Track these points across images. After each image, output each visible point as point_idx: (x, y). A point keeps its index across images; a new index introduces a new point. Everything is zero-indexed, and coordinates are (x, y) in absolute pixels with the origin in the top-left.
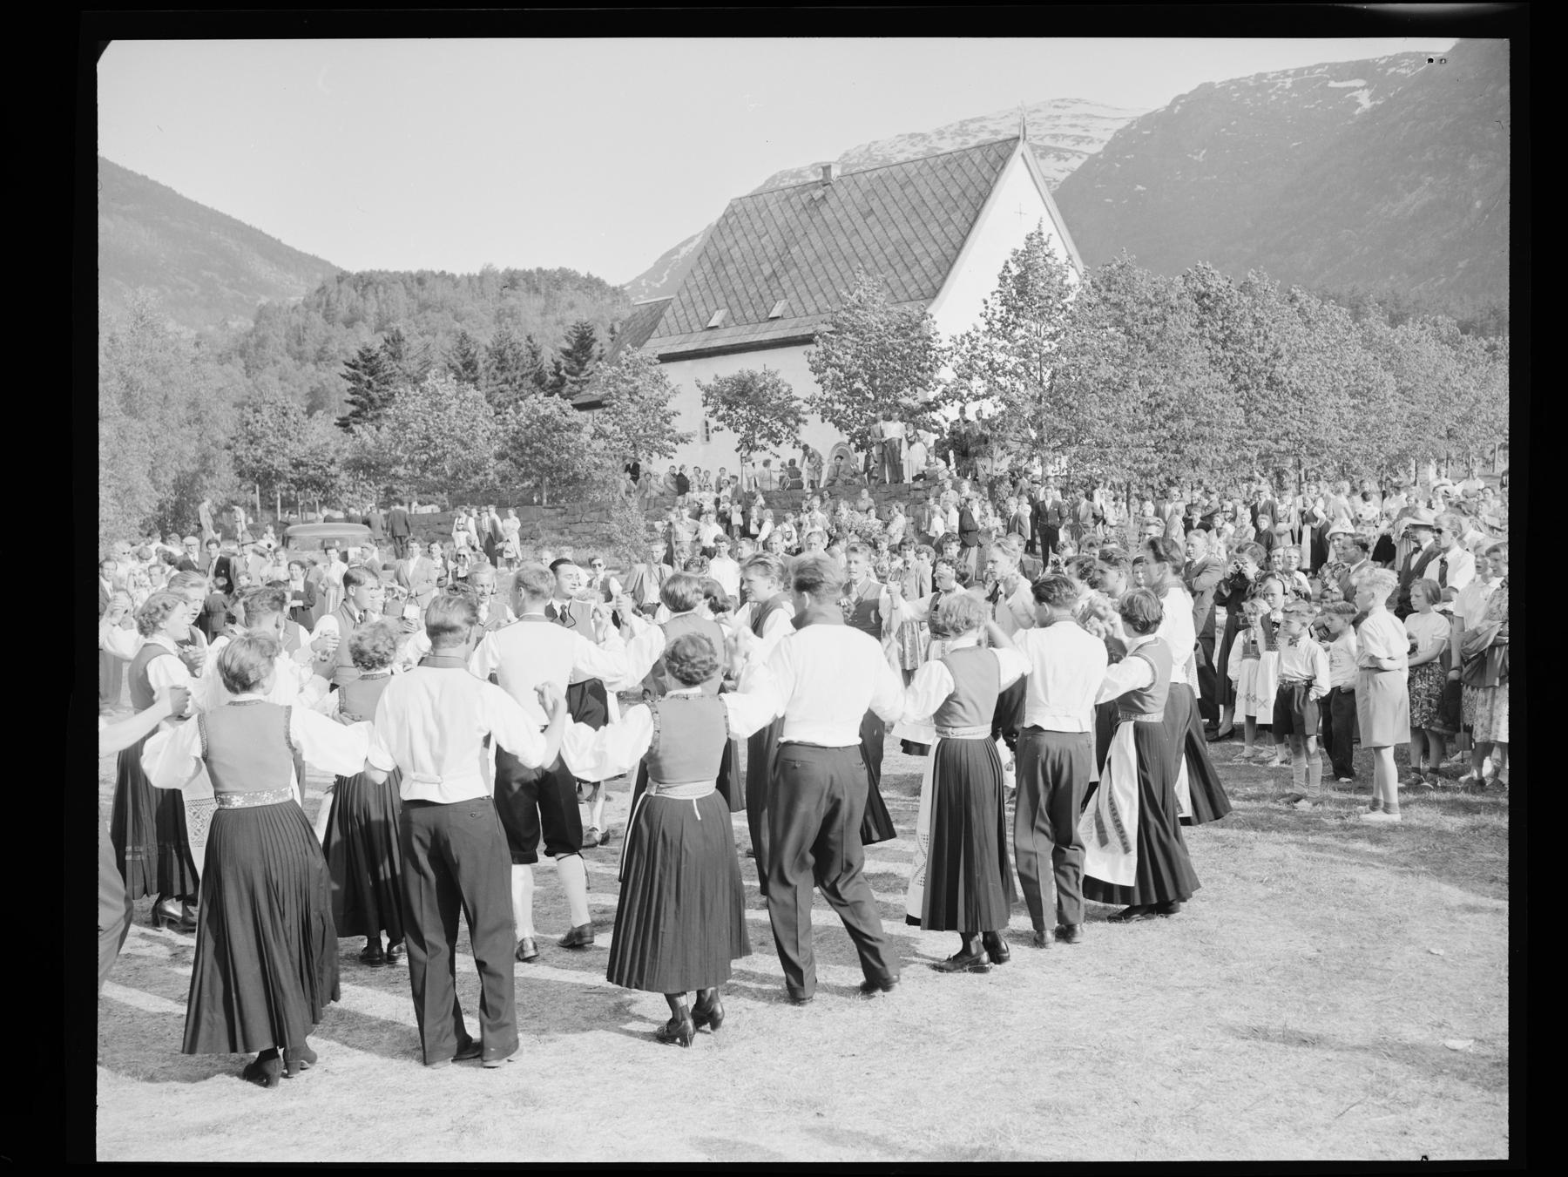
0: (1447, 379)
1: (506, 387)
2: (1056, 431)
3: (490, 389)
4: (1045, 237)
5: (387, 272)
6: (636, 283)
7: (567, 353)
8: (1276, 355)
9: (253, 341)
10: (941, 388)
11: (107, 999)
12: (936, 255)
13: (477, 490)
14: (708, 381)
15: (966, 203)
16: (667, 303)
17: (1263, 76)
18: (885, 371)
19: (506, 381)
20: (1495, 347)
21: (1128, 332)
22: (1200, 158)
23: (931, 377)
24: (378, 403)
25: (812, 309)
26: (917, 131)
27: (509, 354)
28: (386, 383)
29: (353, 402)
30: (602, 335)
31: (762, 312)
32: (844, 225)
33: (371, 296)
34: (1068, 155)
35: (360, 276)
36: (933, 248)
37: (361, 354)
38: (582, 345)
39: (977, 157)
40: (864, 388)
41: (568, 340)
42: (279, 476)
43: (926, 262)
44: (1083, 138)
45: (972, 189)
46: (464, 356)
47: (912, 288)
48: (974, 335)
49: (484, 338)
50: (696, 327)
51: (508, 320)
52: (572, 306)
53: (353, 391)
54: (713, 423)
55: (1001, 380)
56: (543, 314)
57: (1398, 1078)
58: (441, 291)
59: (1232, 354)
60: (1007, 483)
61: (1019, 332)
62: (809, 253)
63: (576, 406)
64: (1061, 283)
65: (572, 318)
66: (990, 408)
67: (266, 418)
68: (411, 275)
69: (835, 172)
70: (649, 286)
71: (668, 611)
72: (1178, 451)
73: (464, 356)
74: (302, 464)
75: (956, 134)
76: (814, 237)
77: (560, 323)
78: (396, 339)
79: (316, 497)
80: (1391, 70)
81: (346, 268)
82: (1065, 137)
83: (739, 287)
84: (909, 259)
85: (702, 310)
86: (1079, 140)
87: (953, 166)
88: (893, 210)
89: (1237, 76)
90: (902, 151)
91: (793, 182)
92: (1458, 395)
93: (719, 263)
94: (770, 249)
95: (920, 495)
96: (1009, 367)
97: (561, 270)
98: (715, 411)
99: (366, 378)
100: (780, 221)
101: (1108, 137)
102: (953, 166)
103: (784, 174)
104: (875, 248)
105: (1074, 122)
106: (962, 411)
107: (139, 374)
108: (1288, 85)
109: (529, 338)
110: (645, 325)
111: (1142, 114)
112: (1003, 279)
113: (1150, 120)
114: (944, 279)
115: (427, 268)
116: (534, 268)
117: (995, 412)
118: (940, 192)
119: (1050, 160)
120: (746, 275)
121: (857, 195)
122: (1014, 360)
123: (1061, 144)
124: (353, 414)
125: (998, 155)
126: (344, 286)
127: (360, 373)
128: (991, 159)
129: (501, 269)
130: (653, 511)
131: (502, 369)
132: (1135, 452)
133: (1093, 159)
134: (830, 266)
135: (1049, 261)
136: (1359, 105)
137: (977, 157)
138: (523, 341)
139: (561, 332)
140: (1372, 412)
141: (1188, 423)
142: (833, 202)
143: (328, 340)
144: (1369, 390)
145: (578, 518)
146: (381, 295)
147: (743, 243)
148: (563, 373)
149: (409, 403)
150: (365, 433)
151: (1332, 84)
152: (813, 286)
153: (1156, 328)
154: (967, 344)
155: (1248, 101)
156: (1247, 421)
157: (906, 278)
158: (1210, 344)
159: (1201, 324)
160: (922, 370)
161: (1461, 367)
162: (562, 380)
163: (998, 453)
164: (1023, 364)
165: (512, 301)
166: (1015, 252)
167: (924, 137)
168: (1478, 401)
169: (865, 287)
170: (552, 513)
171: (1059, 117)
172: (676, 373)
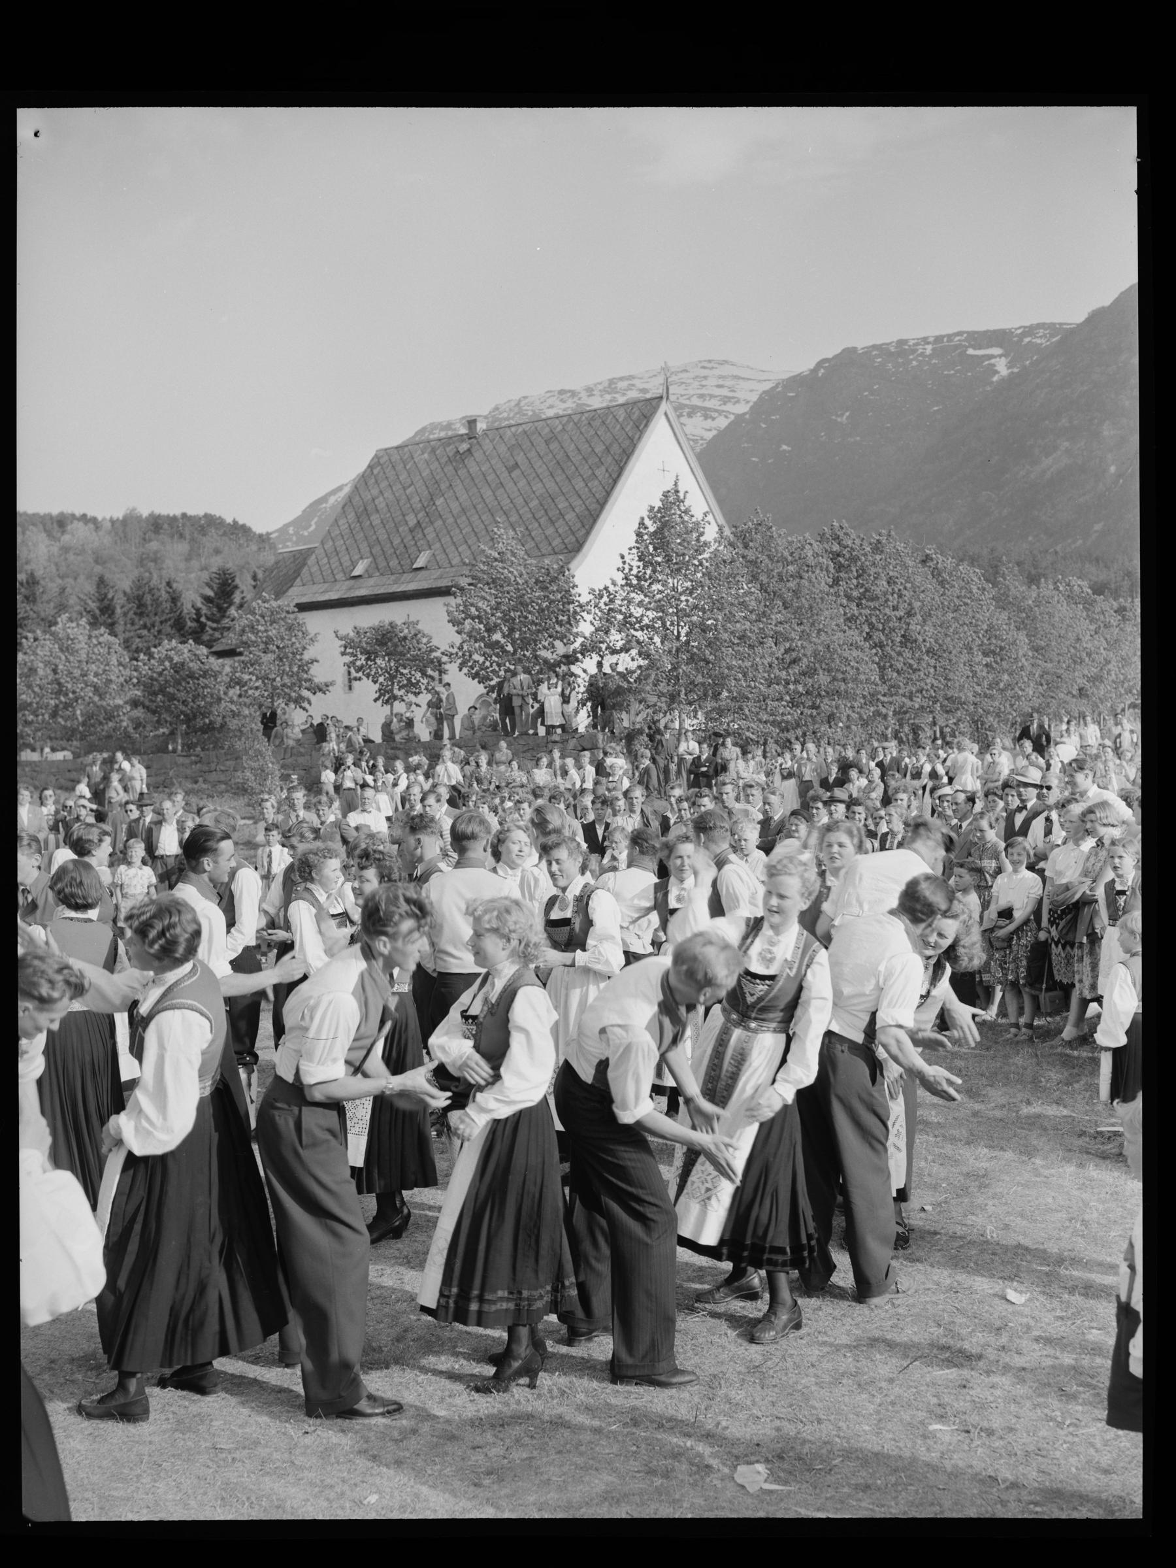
0: (1078, 640)
1: (145, 632)
2: (692, 686)
3: (128, 635)
4: (681, 495)
6: (283, 530)
7: (208, 600)
8: (910, 614)
10: (580, 640)
13: (109, 737)
14: (347, 630)
15: (610, 459)
16: (310, 551)
18: (524, 624)
20: (1125, 609)
21: (763, 588)
23: (569, 630)
26: (567, 388)
27: (148, 599)
30: (244, 584)
32: (489, 478)
34: (715, 415)
36: (577, 503)
38: (224, 590)
40: (503, 641)
43: (570, 516)
45: (616, 446)
48: (612, 589)
49: (123, 583)
50: (340, 576)
51: (152, 564)
52: (217, 552)
55: (639, 634)
56: (188, 559)
57: (964, 1332)
58: (79, 534)
61: (656, 587)
62: (454, 506)
64: (698, 540)
65: (216, 563)
66: (627, 662)
68: (50, 516)
69: (481, 426)
70: (296, 533)
72: (814, 707)
75: (605, 391)
76: (459, 488)
80: (1027, 340)
82: (712, 396)
83: (383, 536)
84: (553, 513)
85: (346, 560)
86: (726, 400)
87: (597, 423)
88: (538, 464)
89: (879, 342)
91: (443, 434)
92: (1089, 655)
93: (363, 513)
96: (646, 621)
97: (206, 515)
101: (754, 398)
102: (597, 423)
103: (433, 427)
104: (519, 501)
105: (721, 382)
106: (600, 665)
108: (928, 352)
109: (169, 584)
110: (291, 569)
111: (786, 376)
112: (639, 534)
114: (588, 533)
117: (633, 665)
118: (585, 447)
119: (698, 419)
121: (502, 449)
123: (708, 404)
125: (642, 414)
128: (635, 417)
130: (289, 761)
133: (739, 418)
134: (475, 518)
135: (686, 518)
136: (997, 372)
137: (621, 415)
139: (205, 576)
140: (1004, 671)
142: (478, 455)
144: (1002, 649)
145: (213, 766)
148: (203, 619)
151: (971, 352)
152: (458, 538)
153: (792, 584)
154: (605, 599)
156: (882, 677)
157: (550, 531)
158: (845, 602)
159: (836, 582)
160: (560, 623)
161: (1093, 627)
162: (203, 626)
163: (635, 706)
164: (660, 618)
165: (154, 545)
166: (652, 509)
167: (573, 394)
168: (1108, 662)
169: (507, 538)
170: (187, 761)
171: (705, 378)
172: (314, 622)
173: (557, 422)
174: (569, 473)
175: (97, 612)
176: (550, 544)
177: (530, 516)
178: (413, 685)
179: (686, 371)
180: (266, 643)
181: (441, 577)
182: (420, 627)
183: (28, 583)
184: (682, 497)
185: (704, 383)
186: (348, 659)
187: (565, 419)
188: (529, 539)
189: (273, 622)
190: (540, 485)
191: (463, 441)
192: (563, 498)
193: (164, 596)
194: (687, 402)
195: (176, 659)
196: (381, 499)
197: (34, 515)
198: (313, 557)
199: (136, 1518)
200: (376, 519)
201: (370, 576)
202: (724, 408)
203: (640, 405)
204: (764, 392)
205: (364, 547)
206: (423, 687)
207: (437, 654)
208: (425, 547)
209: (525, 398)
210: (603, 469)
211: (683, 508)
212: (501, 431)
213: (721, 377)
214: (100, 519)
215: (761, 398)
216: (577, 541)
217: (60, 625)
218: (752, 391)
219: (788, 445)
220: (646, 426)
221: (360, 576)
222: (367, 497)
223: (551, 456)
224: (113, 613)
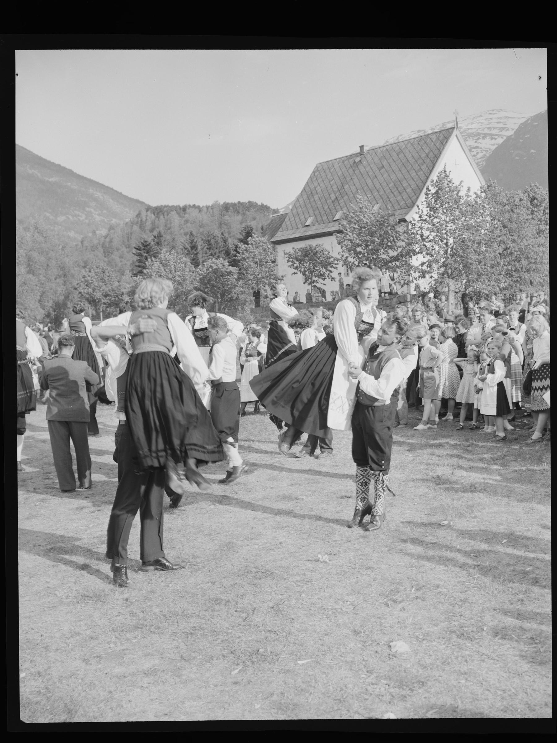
4: (447, 173)
9: (108, 240)
11: (549, 589)
12: (413, 186)
15: (428, 160)
27: (213, 241)
29: (139, 266)
32: (370, 174)
33: (162, 217)
34: (496, 137)
35: (156, 208)
36: (412, 183)
39: (434, 137)
41: (241, 234)
43: (409, 190)
47: (402, 203)
50: (300, 226)
52: (254, 219)
58: (194, 213)
62: (353, 188)
64: (457, 195)
69: (366, 149)
73: (191, 243)
76: (356, 180)
82: (494, 128)
84: (401, 189)
85: (302, 218)
86: (502, 129)
88: (393, 165)
95: (388, 302)
96: (431, 238)
97: (249, 202)
98: (293, 265)
99: (145, 254)
101: (516, 127)
104: (384, 184)
105: (499, 120)
107: (35, 255)
116: (236, 202)
118: (416, 156)
119: (488, 140)
121: (376, 159)
122: (434, 234)
125: (444, 136)
126: (149, 213)
127: (142, 252)
128: (441, 139)
129: (222, 203)
133: (509, 138)
135: (450, 185)
137: (434, 137)
141: (524, 262)
142: (364, 163)
146: (166, 217)
147: (322, 185)
171: (491, 119)
173: (403, 143)
174: (408, 169)
175: (190, 249)
176: (399, 204)
178: (321, 274)
179: (481, 116)
180: (253, 258)
182: (323, 246)
183: (158, 236)
184: (448, 174)
185: (490, 122)
186: (290, 263)
187: (407, 142)
188: (389, 203)
189: (257, 247)
190: (394, 176)
191: (357, 156)
192: (405, 181)
193: (220, 240)
194: (482, 132)
195: (215, 267)
196: (319, 187)
197: (172, 206)
198: (287, 217)
199: (269, 719)
202: (501, 133)
203: (443, 132)
204: (521, 124)
205: (311, 211)
206: (326, 276)
207: (332, 260)
208: (340, 209)
209: (401, 135)
210: (425, 166)
211: (449, 180)
212: (376, 150)
213: (499, 118)
214: (201, 206)
215: (520, 127)
216: (412, 202)
217: (162, 255)
218: (515, 124)
219: (534, 150)
220: (446, 142)
221: (309, 225)
222: (312, 187)
224: (197, 249)
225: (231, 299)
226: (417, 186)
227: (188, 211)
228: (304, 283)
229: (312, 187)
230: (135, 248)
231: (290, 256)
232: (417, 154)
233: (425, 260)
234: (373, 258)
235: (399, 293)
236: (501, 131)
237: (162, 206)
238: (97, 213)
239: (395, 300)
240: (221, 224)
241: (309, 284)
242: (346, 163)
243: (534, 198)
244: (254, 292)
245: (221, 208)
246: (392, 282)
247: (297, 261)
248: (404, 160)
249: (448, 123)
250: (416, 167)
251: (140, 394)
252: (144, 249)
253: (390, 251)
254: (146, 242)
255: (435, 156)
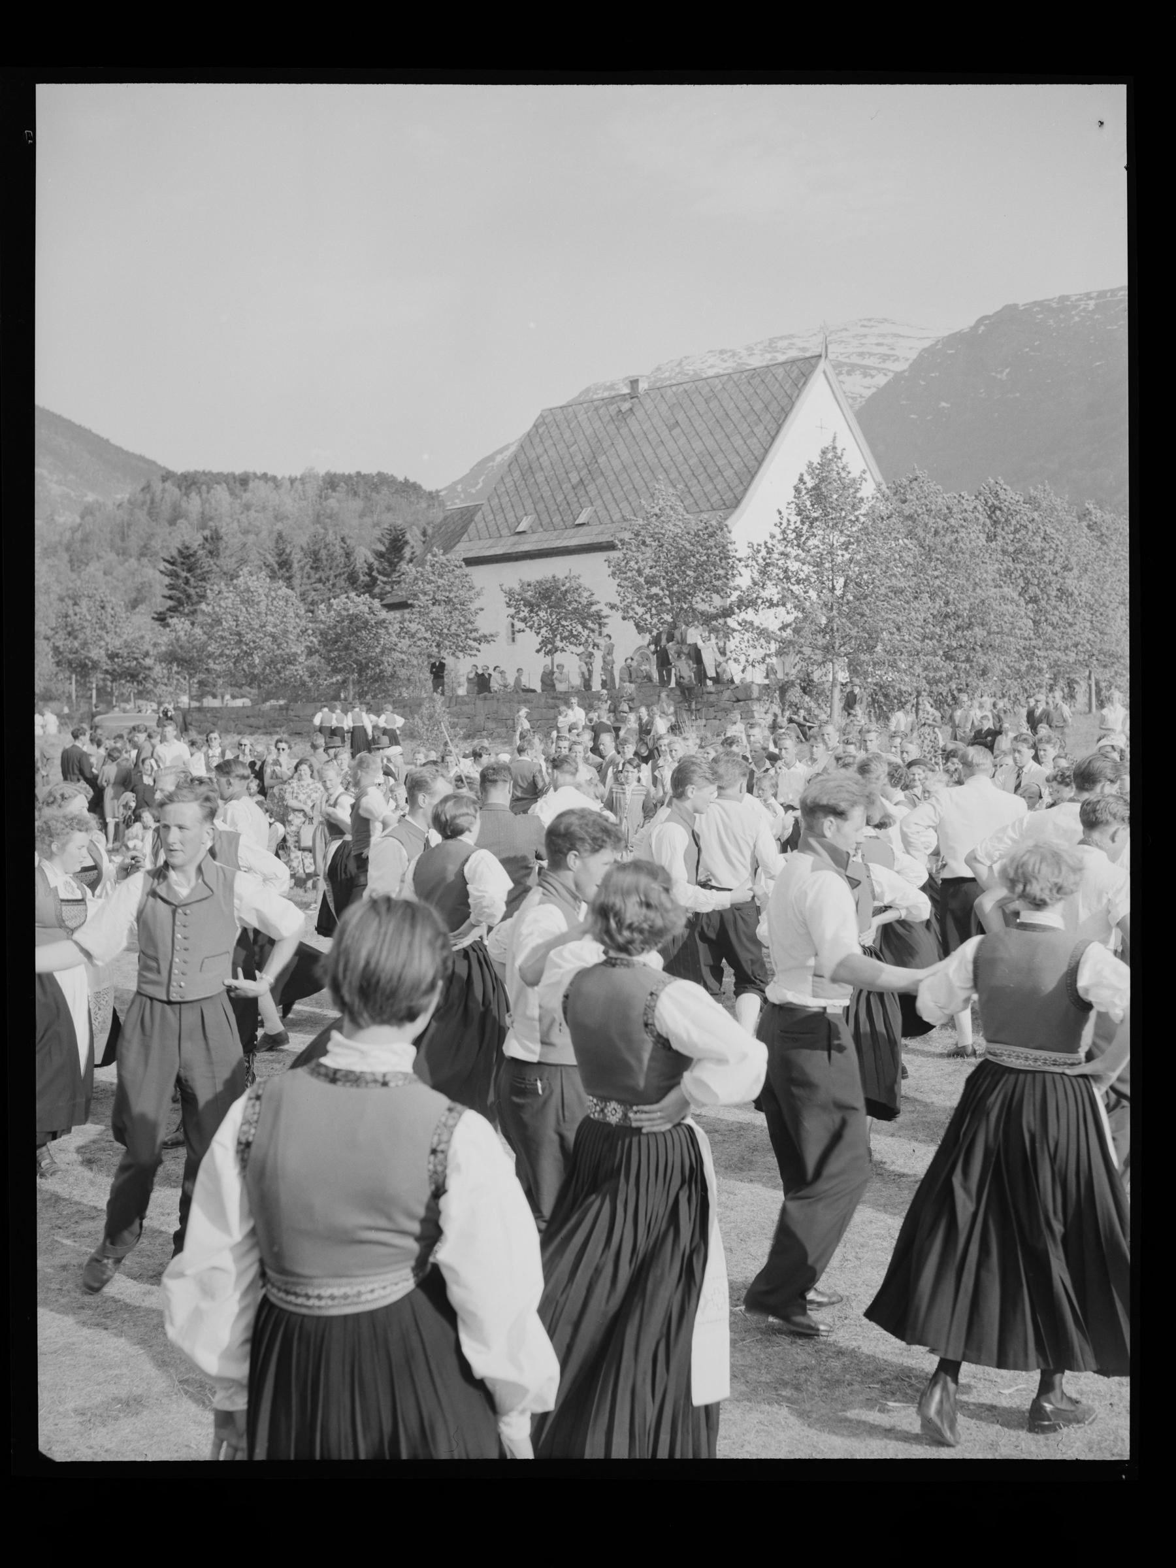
3: (304, 588)
4: (839, 452)
5: (210, 473)
6: (452, 488)
7: (380, 555)
8: (1066, 568)
9: (79, 535)
16: (477, 508)
17: (1067, 298)
18: (686, 580)
19: (320, 580)
22: (1004, 376)
23: (726, 585)
24: (195, 599)
25: (617, 516)
27: (323, 554)
28: (203, 579)
29: (170, 598)
30: (413, 537)
31: (569, 519)
32: (650, 437)
33: (193, 495)
34: (873, 372)
35: (185, 476)
36: (736, 460)
37: (180, 552)
39: (780, 372)
41: (380, 541)
42: (95, 665)
43: (729, 473)
44: (889, 356)
46: (280, 555)
47: (715, 498)
50: (505, 532)
52: (389, 509)
53: (171, 587)
54: (519, 625)
56: (362, 515)
58: (260, 491)
59: (1023, 566)
60: (798, 688)
62: (616, 463)
63: (384, 606)
65: (388, 520)
67: (85, 610)
68: (234, 476)
69: (643, 386)
71: (542, 818)
72: (968, 660)
73: (280, 555)
74: (117, 655)
76: (621, 447)
77: (376, 525)
78: (216, 537)
79: (130, 688)
81: (171, 467)
82: (871, 354)
84: (712, 470)
85: (510, 516)
86: (885, 358)
87: (757, 381)
90: (712, 366)
91: (606, 394)
93: (528, 471)
94: (578, 458)
96: (802, 576)
97: (379, 474)
99: (184, 574)
100: (589, 432)
101: (913, 355)
102: (757, 381)
104: (679, 459)
105: (880, 340)
108: (1091, 307)
109: (343, 539)
111: (947, 333)
113: (957, 339)
114: (746, 490)
115: (251, 470)
116: (353, 472)
118: (744, 406)
119: (857, 377)
120: (554, 483)
121: (663, 408)
124: (169, 609)
125: (800, 371)
126: (168, 484)
127: (178, 570)
128: (793, 376)
129: (322, 472)
131: (309, 565)
132: (925, 659)
133: (898, 376)
135: (843, 474)
137: (780, 372)
138: (338, 542)
139: (377, 532)
141: (979, 632)
142: (640, 413)
143: (151, 536)
146: (204, 495)
147: (552, 452)
148: (375, 573)
149: (221, 600)
150: (179, 623)
152: (619, 494)
155: (1051, 322)
157: (709, 488)
158: (1000, 557)
162: (374, 580)
171: (865, 336)
172: (481, 576)
173: (717, 381)
174: (728, 431)
175: (276, 567)
177: (689, 473)
179: (846, 330)
181: (602, 533)
182: (581, 581)
187: (726, 378)
188: (688, 496)
190: (700, 443)
191: (625, 400)
194: (847, 360)
196: (546, 457)
198: (480, 513)
200: (540, 476)
201: (533, 532)
202: (882, 366)
204: (925, 350)
205: (528, 503)
209: (686, 358)
210: (761, 427)
212: (662, 391)
213: (883, 336)
214: (279, 477)
215: (920, 356)
220: (805, 383)
221: (524, 532)
223: (710, 414)
224: (290, 567)
225: (379, 678)
226: (746, 466)
227: (251, 485)
228: (538, 651)
229: (532, 455)
230: (165, 560)
231: (510, 594)
232: (746, 404)
233: (789, 619)
234: (682, 609)
235: (737, 681)
236: (884, 361)
237: (196, 472)
238: (55, 478)
239: (727, 694)
240: (318, 516)
241: (547, 654)
242: (601, 411)
243: (994, 509)
244: (433, 665)
245: (321, 483)
246: (721, 659)
247: (525, 606)
248: (720, 414)
249: (781, 338)
250: (744, 428)
251: (1052, 1149)
252: (183, 563)
253: (715, 596)
254: (187, 548)
255: (783, 409)
